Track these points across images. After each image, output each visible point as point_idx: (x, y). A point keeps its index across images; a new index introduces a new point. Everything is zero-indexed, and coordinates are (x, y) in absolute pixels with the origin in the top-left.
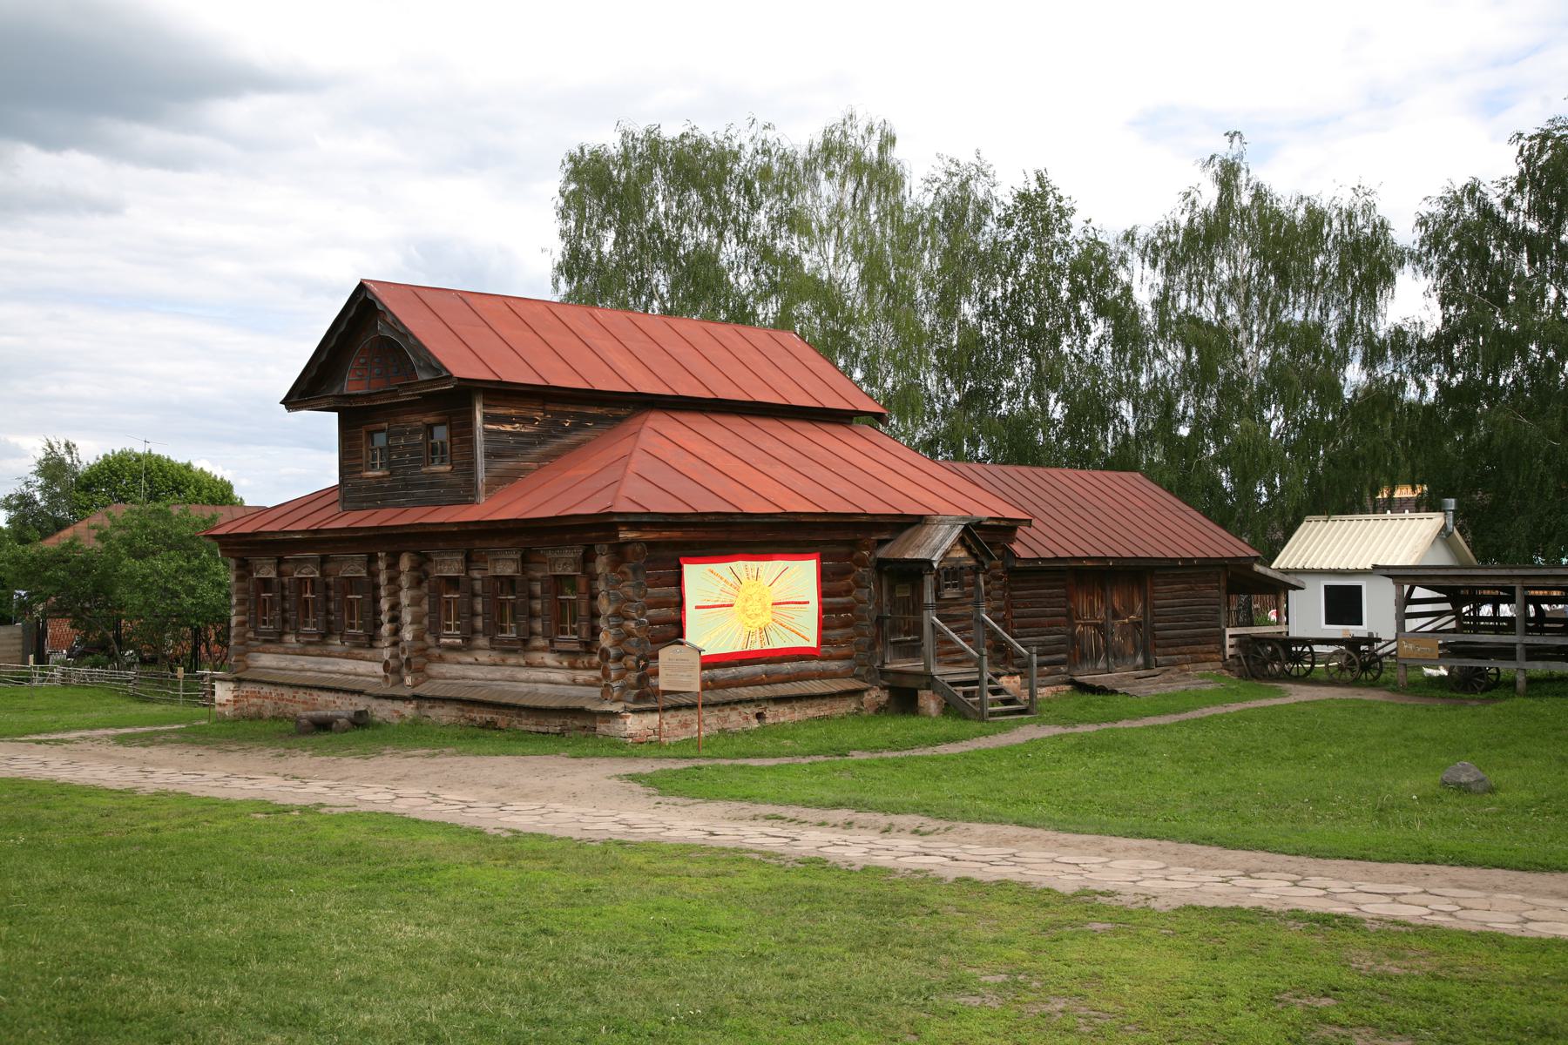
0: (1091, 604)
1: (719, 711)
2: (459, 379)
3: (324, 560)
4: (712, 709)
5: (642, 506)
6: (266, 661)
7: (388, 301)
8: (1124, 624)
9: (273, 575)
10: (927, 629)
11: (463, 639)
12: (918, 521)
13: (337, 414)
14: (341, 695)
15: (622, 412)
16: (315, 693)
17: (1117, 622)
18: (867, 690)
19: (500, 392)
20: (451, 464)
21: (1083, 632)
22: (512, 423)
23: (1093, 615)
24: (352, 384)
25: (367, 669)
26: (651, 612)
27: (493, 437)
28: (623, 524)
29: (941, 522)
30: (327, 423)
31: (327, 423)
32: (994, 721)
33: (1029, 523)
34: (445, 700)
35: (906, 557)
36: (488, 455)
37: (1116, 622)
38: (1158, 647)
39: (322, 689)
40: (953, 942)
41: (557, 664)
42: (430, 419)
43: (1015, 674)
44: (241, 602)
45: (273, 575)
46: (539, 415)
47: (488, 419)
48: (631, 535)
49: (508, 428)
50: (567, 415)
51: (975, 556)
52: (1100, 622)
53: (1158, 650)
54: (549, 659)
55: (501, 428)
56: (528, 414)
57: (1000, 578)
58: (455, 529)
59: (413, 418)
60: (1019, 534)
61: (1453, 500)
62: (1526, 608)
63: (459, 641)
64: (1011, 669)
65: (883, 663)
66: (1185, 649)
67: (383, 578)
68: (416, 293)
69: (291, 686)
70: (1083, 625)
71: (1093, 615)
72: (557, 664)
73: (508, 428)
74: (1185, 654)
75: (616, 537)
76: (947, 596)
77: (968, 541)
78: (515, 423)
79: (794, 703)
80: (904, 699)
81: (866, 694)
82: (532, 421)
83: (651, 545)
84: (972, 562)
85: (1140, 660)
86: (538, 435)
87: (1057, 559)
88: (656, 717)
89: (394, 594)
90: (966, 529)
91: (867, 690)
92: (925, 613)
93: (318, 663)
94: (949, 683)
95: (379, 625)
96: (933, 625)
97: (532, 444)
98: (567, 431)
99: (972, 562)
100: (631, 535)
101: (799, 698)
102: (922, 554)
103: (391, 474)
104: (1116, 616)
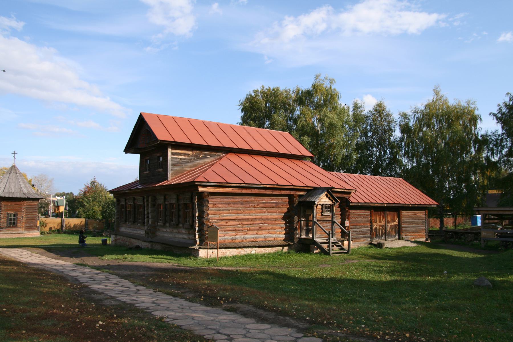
0: (380, 218)
2: (160, 140)
3: (134, 199)
5: (207, 180)
6: (123, 229)
7: (147, 119)
9: (124, 204)
11: (163, 223)
13: (139, 155)
14: (136, 240)
20: (163, 168)
21: (377, 227)
22: (182, 155)
24: (141, 144)
25: (142, 232)
27: (174, 160)
28: (200, 185)
30: (136, 157)
31: (136, 157)
34: (158, 243)
37: (389, 224)
39: (133, 238)
42: (159, 155)
45: (124, 204)
49: (180, 157)
51: (332, 201)
54: (184, 231)
55: (177, 157)
58: (159, 188)
60: (352, 194)
61: (480, 216)
62: (316, 253)
63: (162, 224)
65: (301, 235)
67: (146, 204)
68: (151, 115)
72: (185, 232)
74: (413, 235)
76: (325, 214)
77: (329, 196)
82: (188, 155)
85: (397, 237)
86: (190, 160)
88: (281, 248)
89: (148, 209)
93: (133, 230)
94: (320, 243)
95: (145, 219)
97: (188, 162)
98: (201, 159)
103: (150, 172)
104: (388, 222)
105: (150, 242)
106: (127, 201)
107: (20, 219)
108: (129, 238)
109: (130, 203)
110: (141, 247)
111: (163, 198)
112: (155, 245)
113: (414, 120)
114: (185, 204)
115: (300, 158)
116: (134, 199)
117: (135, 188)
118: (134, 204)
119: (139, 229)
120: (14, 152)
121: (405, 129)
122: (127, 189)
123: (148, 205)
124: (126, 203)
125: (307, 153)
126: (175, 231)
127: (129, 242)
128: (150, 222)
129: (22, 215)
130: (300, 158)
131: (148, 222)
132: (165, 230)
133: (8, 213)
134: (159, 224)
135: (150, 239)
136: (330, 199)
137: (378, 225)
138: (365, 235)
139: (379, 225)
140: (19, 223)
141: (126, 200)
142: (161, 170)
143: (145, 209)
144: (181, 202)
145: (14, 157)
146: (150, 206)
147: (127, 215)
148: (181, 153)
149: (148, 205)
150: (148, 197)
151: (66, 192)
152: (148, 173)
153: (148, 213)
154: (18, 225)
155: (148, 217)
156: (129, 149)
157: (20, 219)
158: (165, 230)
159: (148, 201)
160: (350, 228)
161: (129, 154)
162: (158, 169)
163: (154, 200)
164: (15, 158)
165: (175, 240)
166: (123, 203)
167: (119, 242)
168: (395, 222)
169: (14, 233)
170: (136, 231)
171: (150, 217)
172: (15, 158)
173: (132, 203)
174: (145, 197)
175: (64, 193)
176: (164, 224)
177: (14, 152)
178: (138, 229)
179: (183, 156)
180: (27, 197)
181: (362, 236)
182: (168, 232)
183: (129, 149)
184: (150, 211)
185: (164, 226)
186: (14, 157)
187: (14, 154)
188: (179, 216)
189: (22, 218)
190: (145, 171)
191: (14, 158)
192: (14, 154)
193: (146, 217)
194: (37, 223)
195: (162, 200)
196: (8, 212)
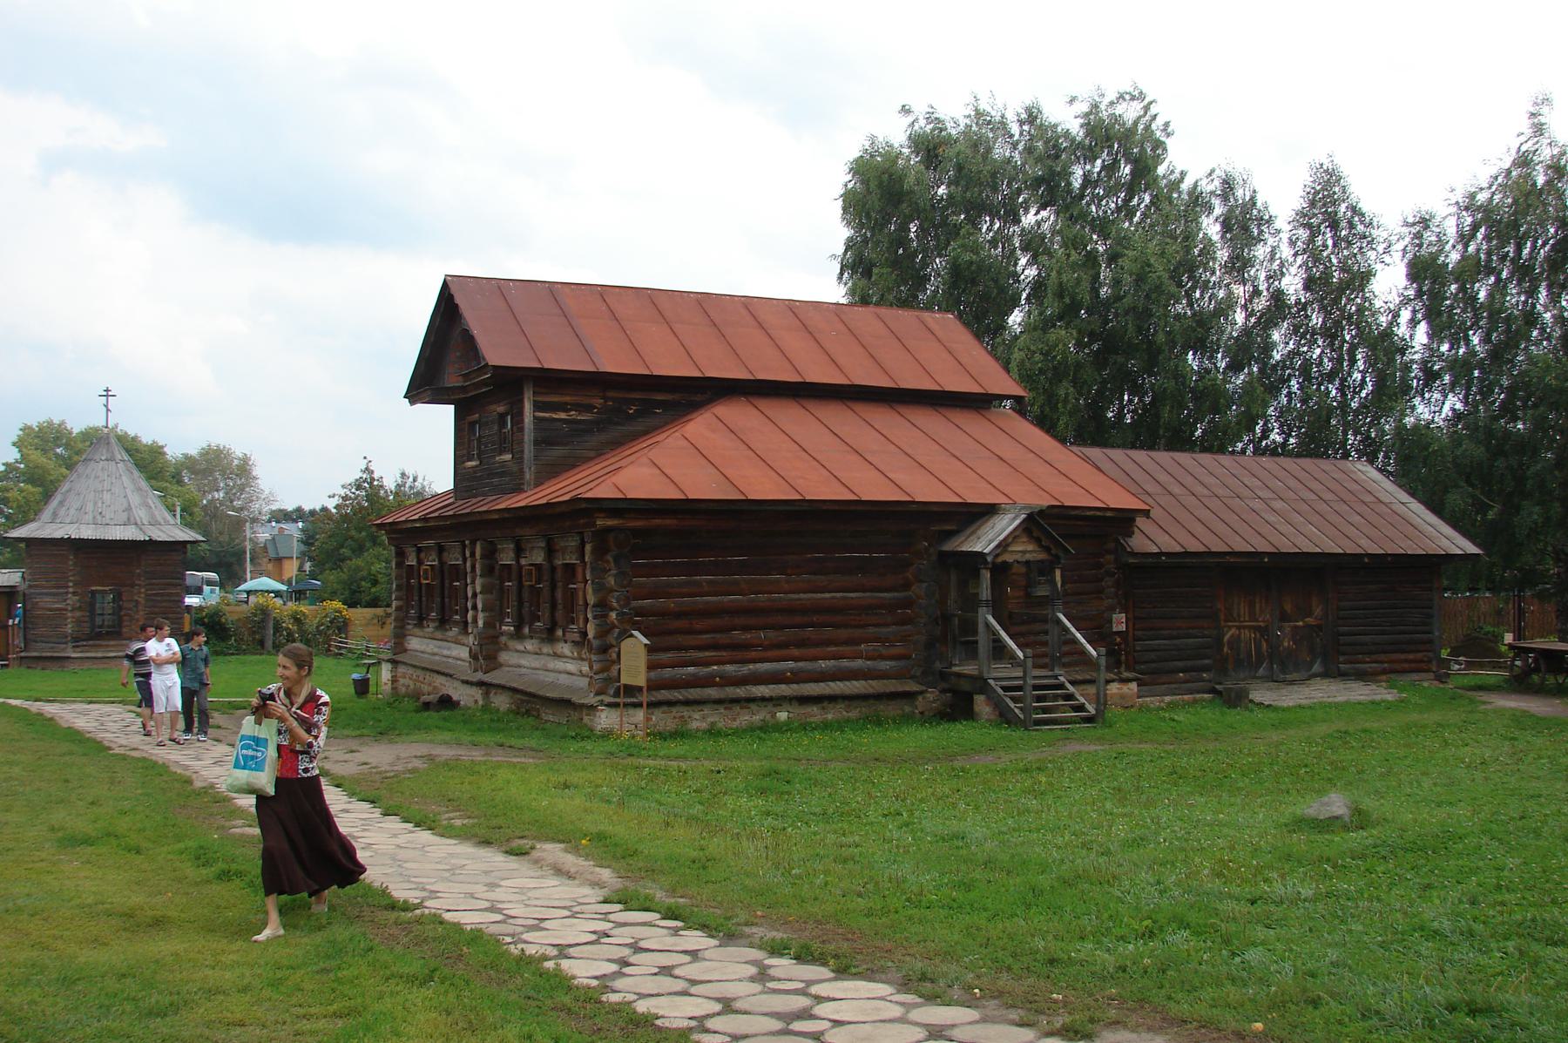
1: (726, 709)
4: (716, 706)
8: (1296, 627)
9: (414, 563)
10: (981, 628)
12: (990, 510)
15: (698, 398)
16: (436, 676)
17: (1287, 626)
18: (921, 693)
19: (548, 380)
20: (512, 453)
21: (1239, 635)
22: (566, 411)
23: (1253, 618)
24: (452, 379)
26: (634, 603)
29: (1005, 512)
30: (442, 417)
31: (442, 417)
32: (1037, 730)
33: (1146, 513)
35: (964, 549)
36: (536, 443)
38: (1343, 654)
39: (438, 672)
40: (470, 1022)
41: (570, 654)
42: (501, 409)
43: (1128, 680)
44: (399, 587)
46: (598, 402)
47: (538, 406)
48: (610, 523)
49: (563, 416)
50: (632, 402)
51: (1047, 549)
52: (1262, 624)
53: (1341, 659)
55: (555, 416)
56: (586, 401)
57: (1113, 575)
58: (497, 517)
59: (493, 407)
64: (1126, 675)
66: (1382, 657)
67: (468, 564)
69: (424, 669)
70: (1239, 628)
71: (1253, 618)
72: (570, 654)
73: (563, 416)
75: (594, 525)
78: (571, 410)
79: (825, 704)
80: (958, 707)
81: (920, 698)
82: (589, 408)
83: (636, 532)
84: (1042, 556)
87: (1187, 554)
89: (473, 582)
90: (1030, 518)
91: (921, 693)
92: (980, 610)
96: (987, 625)
98: (630, 418)
99: (1042, 556)
100: (610, 523)
101: (832, 698)
102: (978, 548)
105: (480, 684)
106: (422, 555)
107: (130, 609)
108: (428, 674)
109: (431, 561)
110: (458, 703)
111: (512, 546)
112: (495, 693)
113: (639, 458)
114: (570, 569)
115: (979, 402)
116: (441, 550)
117: (436, 514)
118: (442, 563)
119: (456, 643)
120: (107, 390)
121: (1423, 270)
122: (416, 517)
123: (473, 567)
124: (420, 562)
125: (1003, 383)
126: (545, 650)
127: (430, 685)
128: (481, 623)
129: (136, 598)
130: (979, 402)
131: (475, 621)
132: (521, 647)
133: (93, 592)
134: (504, 627)
135: (479, 676)
136: (1041, 546)
137: (1245, 627)
138: (1190, 663)
139: (1250, 627)
140: (128, 623)
141: (419, 550)
142: (508, 457)
143: (469, 581)
144: (558, 562)
145: (106, 406)
146: (478, 572)
147: (424, 599)
148: (566, 404)
149: (473, 567)
150: (473, 543)
151: (307, 507)
152: (476, 466)
153: (475, 595)
154: (124, 630)
155: (475, 607)
156: (423, 387)
157: (130, 609)
158: (521, 647)
159: (473, 554)
160: (1135, 640)
161: (419, 406)
162: (501, 455)
163: (490, 554)
164: (108, 410)
165: (547, 679)
166: (412, 561)
167: (403, 685)
168: (1310, 614)
169: (1419, 520)
170: (449, 649)
171: (480, 606)
172: (108, 410)
173: (457, 560)
174: (467, 542)
175: (299, 510)
176: (519, 628)
177: (107, 390)
178: (453, 645)
179: (573, 413)
180: (147, 539)
181: (1180, 664)
182: (529, 653)
183: (423, 387)
184: (478, 590)
185: (518, 635)
186: (106, 406)
187: (107, 396)
188: (554, 606)
189: (136, 606)
190: (469, 460)
191: (105, 409)
192: (107, 396)
193: (469, 605)
194: (183, 624)
195: (512, 554)
196: (94, 588)
